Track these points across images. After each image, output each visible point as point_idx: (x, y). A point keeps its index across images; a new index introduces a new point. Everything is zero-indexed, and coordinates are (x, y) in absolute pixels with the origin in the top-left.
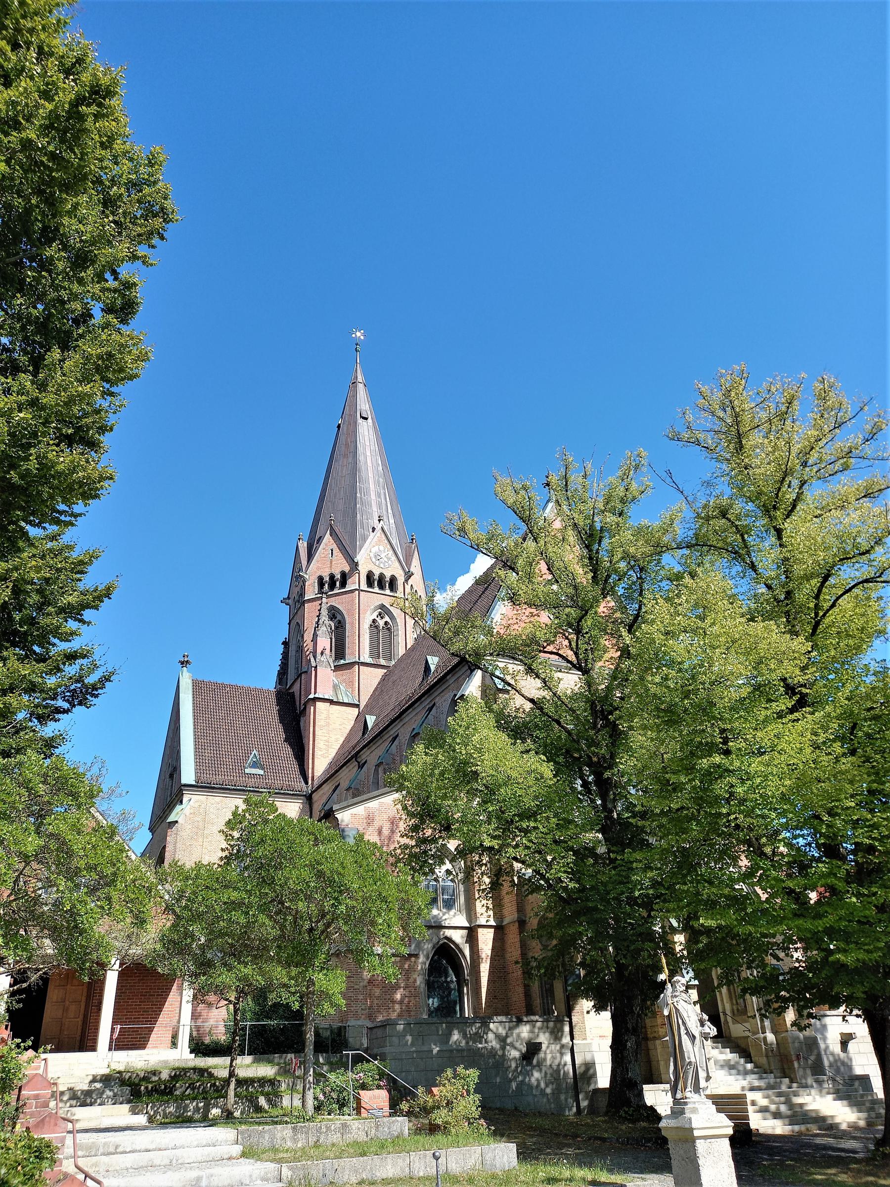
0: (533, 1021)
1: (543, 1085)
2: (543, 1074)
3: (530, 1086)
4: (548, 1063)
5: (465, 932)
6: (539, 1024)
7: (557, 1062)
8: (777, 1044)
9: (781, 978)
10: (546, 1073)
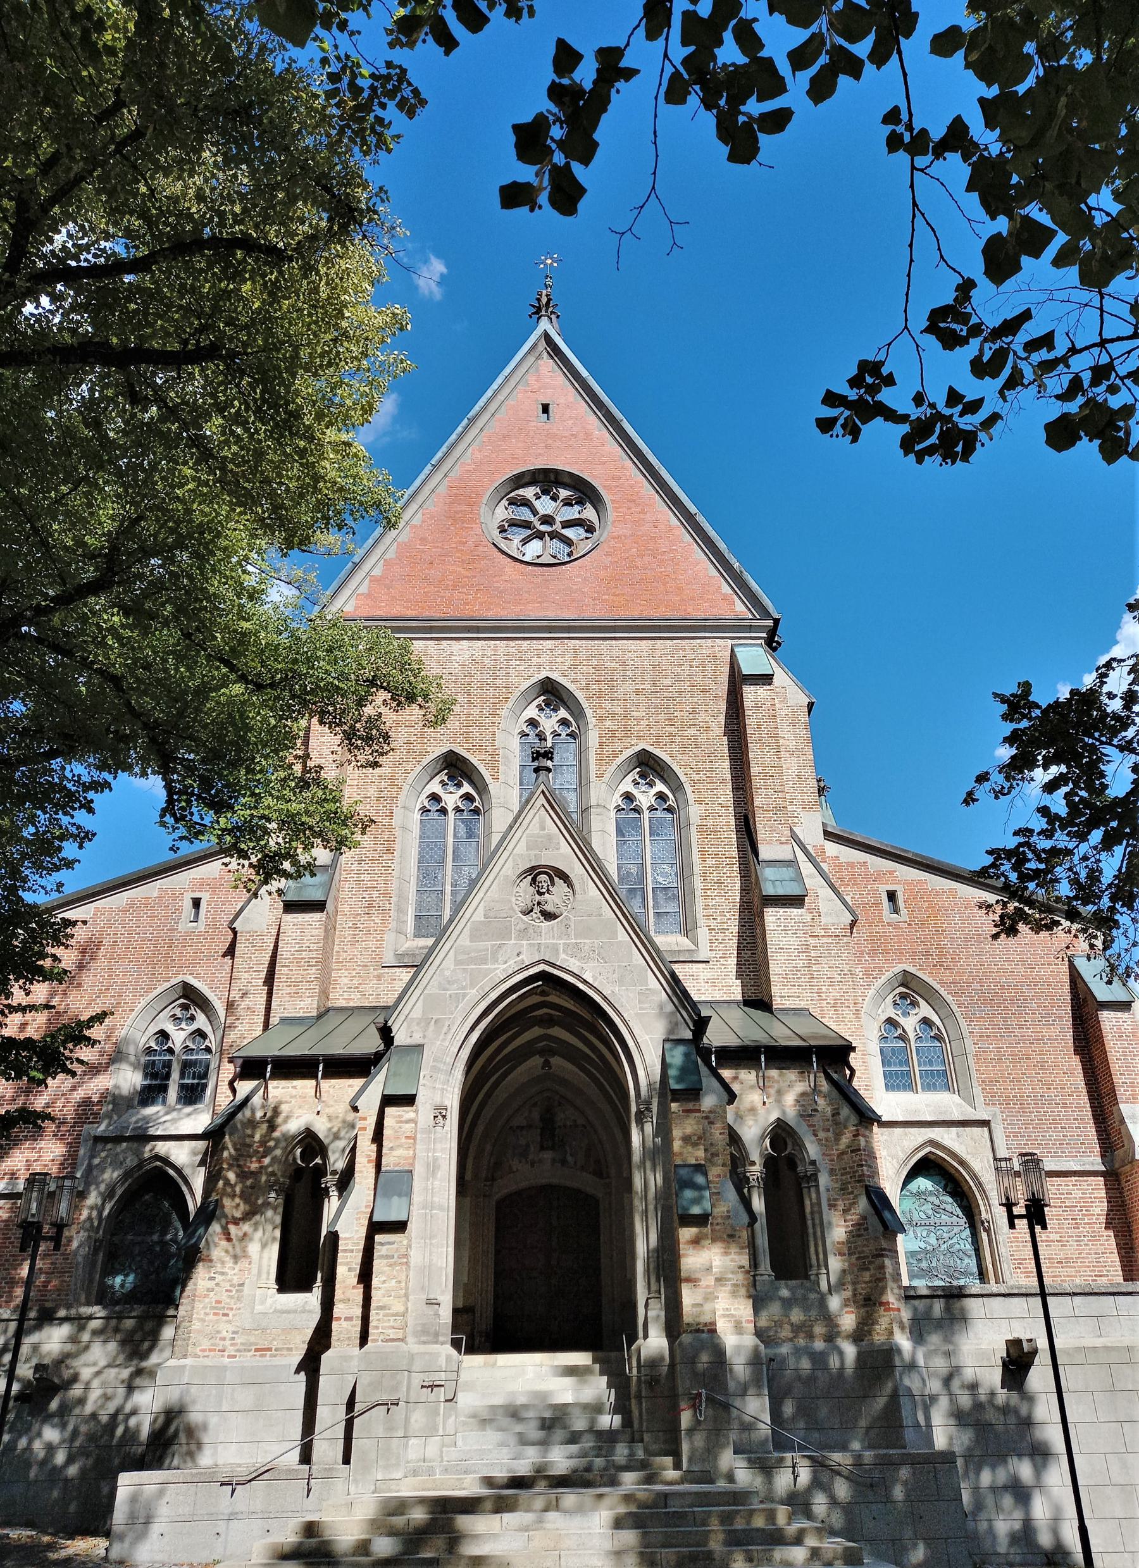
0: (80, 1318)
1: (60, 1458)
2: (67, 1434)
3: (26, 1456)
4: (89, 1408)
5: (201, 1145)
6: (95, 1324)
7: (111, 1407)
8: (672, 1365)
9: (97, 394)
10: (75, 1433)
